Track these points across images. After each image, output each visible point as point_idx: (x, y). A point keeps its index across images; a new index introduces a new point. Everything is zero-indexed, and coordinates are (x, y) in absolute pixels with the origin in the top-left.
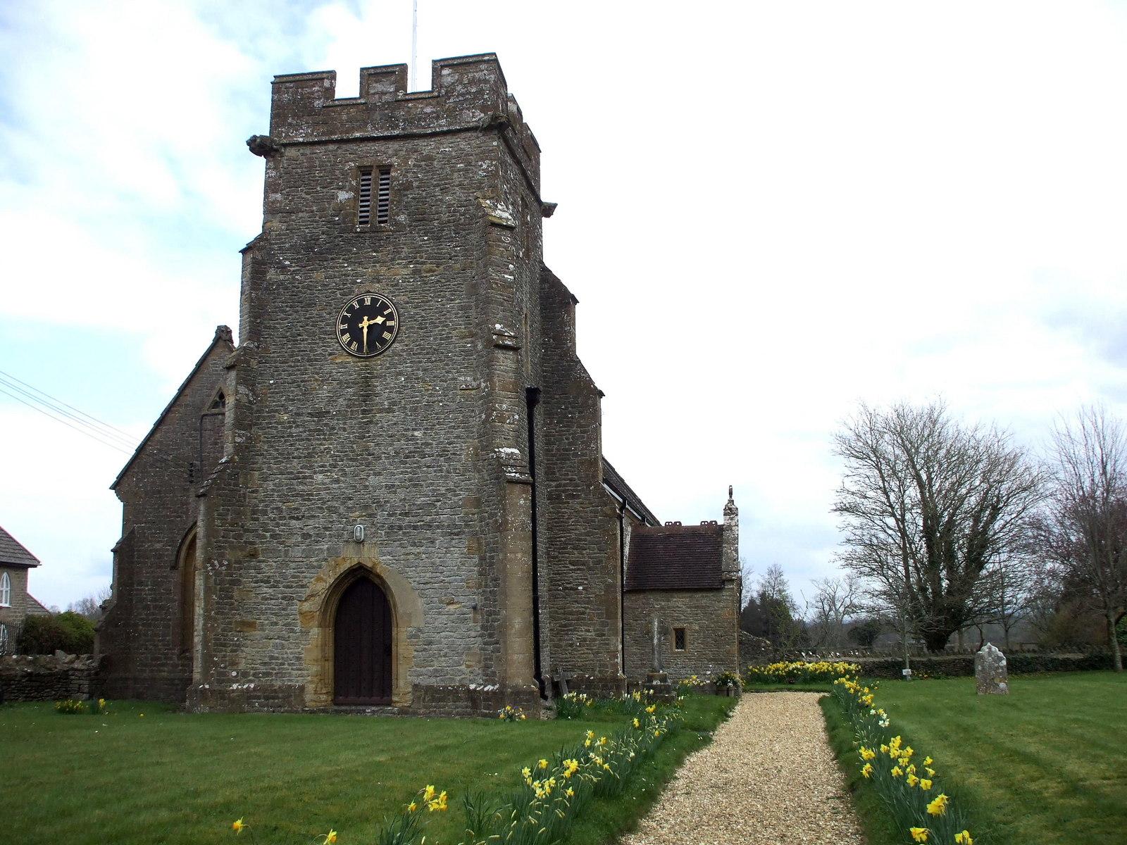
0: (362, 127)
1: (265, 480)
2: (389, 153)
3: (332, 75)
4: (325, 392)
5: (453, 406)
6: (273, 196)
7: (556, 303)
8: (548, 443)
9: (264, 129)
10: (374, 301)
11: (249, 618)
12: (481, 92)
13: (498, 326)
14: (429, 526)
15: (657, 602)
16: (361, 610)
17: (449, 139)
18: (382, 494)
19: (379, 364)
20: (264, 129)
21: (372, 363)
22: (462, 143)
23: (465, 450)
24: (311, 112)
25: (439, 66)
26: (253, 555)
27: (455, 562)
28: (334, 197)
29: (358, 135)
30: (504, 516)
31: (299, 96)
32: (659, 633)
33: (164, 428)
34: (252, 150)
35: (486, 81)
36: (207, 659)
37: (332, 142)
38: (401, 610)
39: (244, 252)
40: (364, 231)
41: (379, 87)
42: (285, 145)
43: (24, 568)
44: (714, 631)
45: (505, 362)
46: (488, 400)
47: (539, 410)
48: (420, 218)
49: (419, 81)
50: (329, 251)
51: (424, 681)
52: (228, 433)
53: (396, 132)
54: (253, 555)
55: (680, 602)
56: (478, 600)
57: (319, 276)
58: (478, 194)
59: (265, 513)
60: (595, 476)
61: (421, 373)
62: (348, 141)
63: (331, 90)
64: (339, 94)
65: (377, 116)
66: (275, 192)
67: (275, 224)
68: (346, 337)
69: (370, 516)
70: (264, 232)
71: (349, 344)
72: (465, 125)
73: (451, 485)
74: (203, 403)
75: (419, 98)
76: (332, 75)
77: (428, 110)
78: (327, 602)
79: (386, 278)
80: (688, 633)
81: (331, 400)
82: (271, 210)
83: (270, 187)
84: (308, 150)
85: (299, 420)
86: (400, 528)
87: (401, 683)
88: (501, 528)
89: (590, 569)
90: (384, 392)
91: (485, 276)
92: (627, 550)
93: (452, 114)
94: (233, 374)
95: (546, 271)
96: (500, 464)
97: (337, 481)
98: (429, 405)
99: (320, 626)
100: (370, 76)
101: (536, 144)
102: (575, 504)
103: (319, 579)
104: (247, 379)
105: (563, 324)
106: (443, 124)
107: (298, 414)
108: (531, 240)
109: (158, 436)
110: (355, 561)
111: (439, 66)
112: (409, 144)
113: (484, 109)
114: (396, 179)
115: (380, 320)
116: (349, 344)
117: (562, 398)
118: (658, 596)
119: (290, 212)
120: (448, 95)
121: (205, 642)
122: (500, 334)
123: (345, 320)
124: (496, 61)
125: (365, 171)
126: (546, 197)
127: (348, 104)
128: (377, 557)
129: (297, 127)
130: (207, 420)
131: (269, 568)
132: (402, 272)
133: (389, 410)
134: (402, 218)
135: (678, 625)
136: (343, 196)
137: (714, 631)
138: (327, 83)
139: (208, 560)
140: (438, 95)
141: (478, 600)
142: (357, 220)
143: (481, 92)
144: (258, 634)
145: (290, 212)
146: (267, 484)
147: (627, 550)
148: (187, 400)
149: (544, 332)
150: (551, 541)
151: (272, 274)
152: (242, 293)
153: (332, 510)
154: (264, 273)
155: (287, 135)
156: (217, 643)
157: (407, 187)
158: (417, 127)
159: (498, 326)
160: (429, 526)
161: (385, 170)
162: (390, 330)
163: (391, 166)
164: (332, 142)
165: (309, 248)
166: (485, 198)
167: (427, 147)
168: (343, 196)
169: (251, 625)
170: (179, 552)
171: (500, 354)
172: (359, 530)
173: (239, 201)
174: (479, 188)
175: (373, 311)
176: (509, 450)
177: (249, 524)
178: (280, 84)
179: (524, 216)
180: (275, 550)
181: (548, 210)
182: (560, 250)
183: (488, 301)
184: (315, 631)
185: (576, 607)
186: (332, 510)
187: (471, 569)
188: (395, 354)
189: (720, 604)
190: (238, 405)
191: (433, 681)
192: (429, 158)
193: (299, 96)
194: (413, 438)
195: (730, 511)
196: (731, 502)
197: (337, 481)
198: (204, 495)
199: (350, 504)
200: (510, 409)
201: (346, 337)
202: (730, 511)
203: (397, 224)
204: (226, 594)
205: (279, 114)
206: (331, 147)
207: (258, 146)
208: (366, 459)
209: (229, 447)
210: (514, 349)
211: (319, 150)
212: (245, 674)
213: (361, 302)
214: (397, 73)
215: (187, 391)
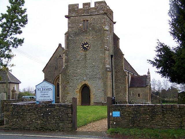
0: (83, 13)
1: (70, 71)
2: (88, 18)
3: (78, 4)
4: (79, 57)
5: (99, 59)
6: (69, 25)
7: (116, 39)
8: (115, 63)
9: (67, 14)
10: (86, 42)
11: (68, 92)
12: (103, 8)
13: (106, 47)
14: (96, 78)
15: (135, 89)
16: (85, 90)
17: (98, 15)
18: (88, 73)
19: (87, 52)
20: (67, 14)
21: (86, 52)
22: (100, 16)
23: (101, 66)
24: (75, 11)
25: (96, 3)
26: (68, 82)
27: (100, 83)
28: (79, 25)
29: (83, 15)
30: (107, 76)
31: (73, 8)
32: (132, 94)
33: (51, 61)
34: (66, 17)
35: (103, 6)
36: (62, 98)
37: (78, 16)
38: (91, 91)
39: (65, 34)
40: (84, 31)
41: (86, 7)
42: (71, 17)
43: (19, 83)
44: (145, 94)
45: (107, 52)
46: (105, 58)
47: (113, 59)
48: (93, 29)
49: (93, 6)
50: (79, 34)
51: (95, 101)
52: (64, 64)
53: (89, 14)
54: (68, 82)
55: (139, 89)
56: (104, 89)
57: (77, 38)
58: (102, 25)
59: (70, 76)
60: (123, 69)
61: (94, 54)
62: (81, 16)
63: (78, 7)
64: (79, 8)
65: (86, 12)
66: (70, 24)
67: (70, 30)
68: (82, 48)
69: (87, 76)
70: (68, 31)
71: (83, 49)
72: (100, 13)
73: (99, 72)
74: (57, 57)
75: (92, 8)
76: (78, 4)
77: (94, 11)
78: (80, 89)
79: (88, 38)
80: (140, 94)
81: (80, 58)
82: (69, 27)
83: (69, 24)
84: (75, 17)
85: (75, 61)
86: (91, 78)
87: (92, 102)
88: (107, 78)
89: (122, 84)
90: (88, 57)
91: (104, 39)
92: (130, 80)
93: (98, 11)
94: (64, 54)
95: (114, 34)
96: (106, 68)
97: (81, 71)
98: (95, 59)
99: (79, 93)
100: (84, 4)
101: (112, 11)
102: (119, 73)
103: (79, 86)
104: (67, 55)
105: (117, 43)
106: (96, 13)
107: (75, 60)
108: (112, 29)
109: (50, 62)
110: (84, 83)
111: (96, 3)
112: (91, 16)
113: (103, 10)
114: (89, 22)
115: (87, 45)
116: (83, 49)
117: (117, 54)
118: (135, 88)
119: (72, 28)
120: (97, 8)
121: (62, 96)
122: (106, 48)
123: (82, 45)
124: (105, 2)
125: (84, 21)
126: (114, 21)
127: (81, 9)
128: (87, 82)
129: (73, 13)
130: (58, 59)
131: (71, 84)
132: (91, 37)
133: (89, 60)
134: (90, 29)
135: (138, 93)
136: (81, 25)
137: (145, 94)
138: (77, 6)
139: (62, 83)
140: (96, 8)
141: (104, 89)
142: (83, 29)
143: (103, 8)
144: (69, 95)
145: (72, 28)
146: (70, 71)
147: (130, 80)
148: (54, 56)
149: (114, 44)
150: (115, 79)
151: (70, 38)
152: (65, 41)
153: (81, 75)
154: (69, 38)
155: (71, 15)
156: (63, 96)
157: (91, 24)
158: (93, 13)
159: (106, 47)
160: (96, 78)
161: (87, 21)
162: (89, 47)
163: (88, 20)
164: (78, 16)
165: (76, 34)
166: (103, 25)
167: (94, 17)
168: (81, 25)
169: (68, 93)
170: (54, 81)
171: (106, 51)
172: (85, 78)
173: (64, 26)
174: (103, 24)
175: (86, 44)
176: (108, 66)
177: (68, 78)
178: (70, 6)
179: (110, 26)
180: (72, 82)
181: (115, 23)
182: (117, 30)
183: (104, 43)
184: (78, 94)
185: (119, 90)
186: (81, 75)
187: (102, 84)
188: (90, 51)
189: (147, 90)
190: (65, 59)
191: (96, 101)
192: (94, 19)
193: (73, 8)
194: (93, 64)
195: (149, 73)
196: (149, 71)
197: (81, 71)
198: (61, 73)
199: (83, 74)
200: (108, 60)
201: (82, 48)
202: (149, 73)
203: (90, 30)
204: (65, 89)
205: (70, 11)
206: (79, 17)
207: (66, 17)
208: (85, 67)
209: (64, 66)
210: (109, 50)
211: (76, 17)
212: (68, 101)
213: (84, 42)
214: (88, 4)
215: (54, 55)
